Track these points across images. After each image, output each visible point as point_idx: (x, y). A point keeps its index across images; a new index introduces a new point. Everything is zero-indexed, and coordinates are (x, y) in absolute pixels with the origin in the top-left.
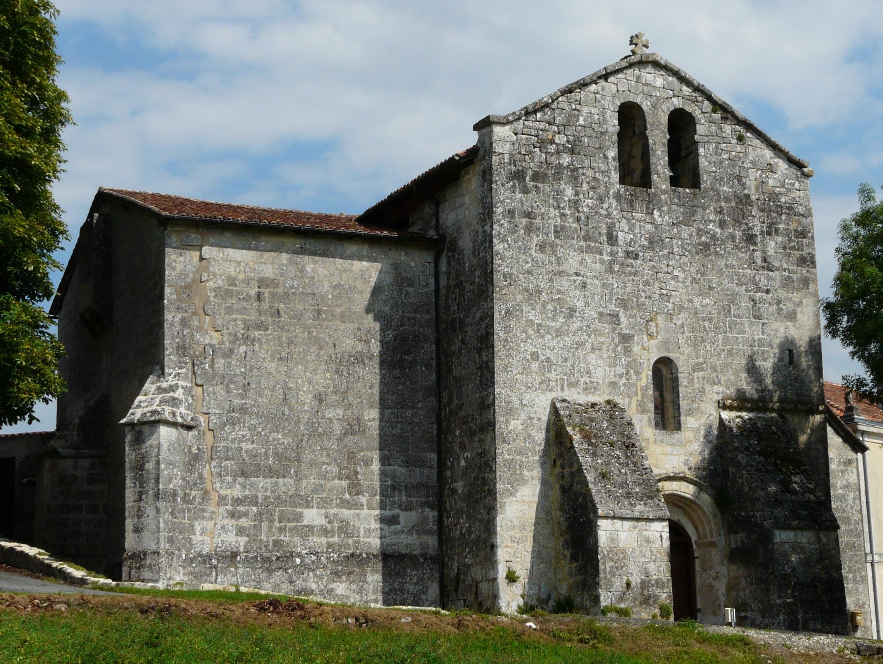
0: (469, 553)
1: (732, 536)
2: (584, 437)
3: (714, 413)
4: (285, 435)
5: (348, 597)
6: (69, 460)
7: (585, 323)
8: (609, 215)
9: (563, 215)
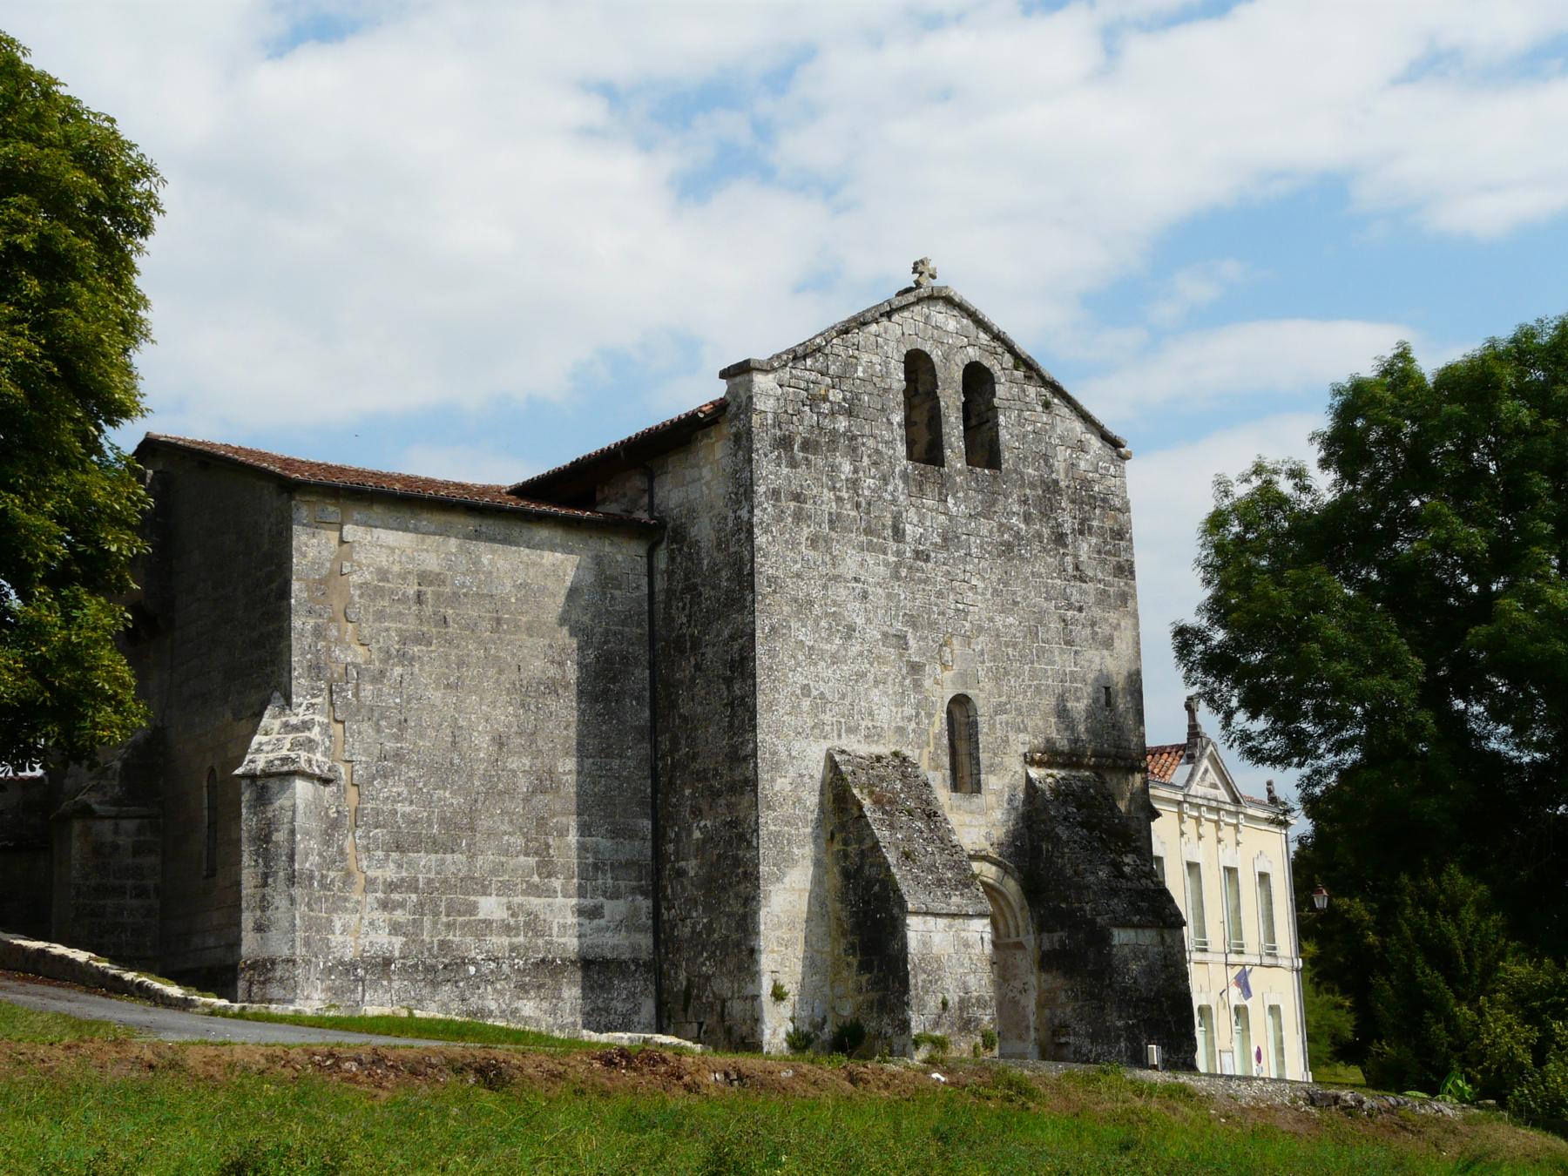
0: (708, 958)
1: (1045, 936)
2: (875, 802)
3: (1020, 770)
4: (454, 793)
5: (538, 1021)
6: (107, 822)
7: (866, 646)
8: (894, 501)
9: (839, 499)
